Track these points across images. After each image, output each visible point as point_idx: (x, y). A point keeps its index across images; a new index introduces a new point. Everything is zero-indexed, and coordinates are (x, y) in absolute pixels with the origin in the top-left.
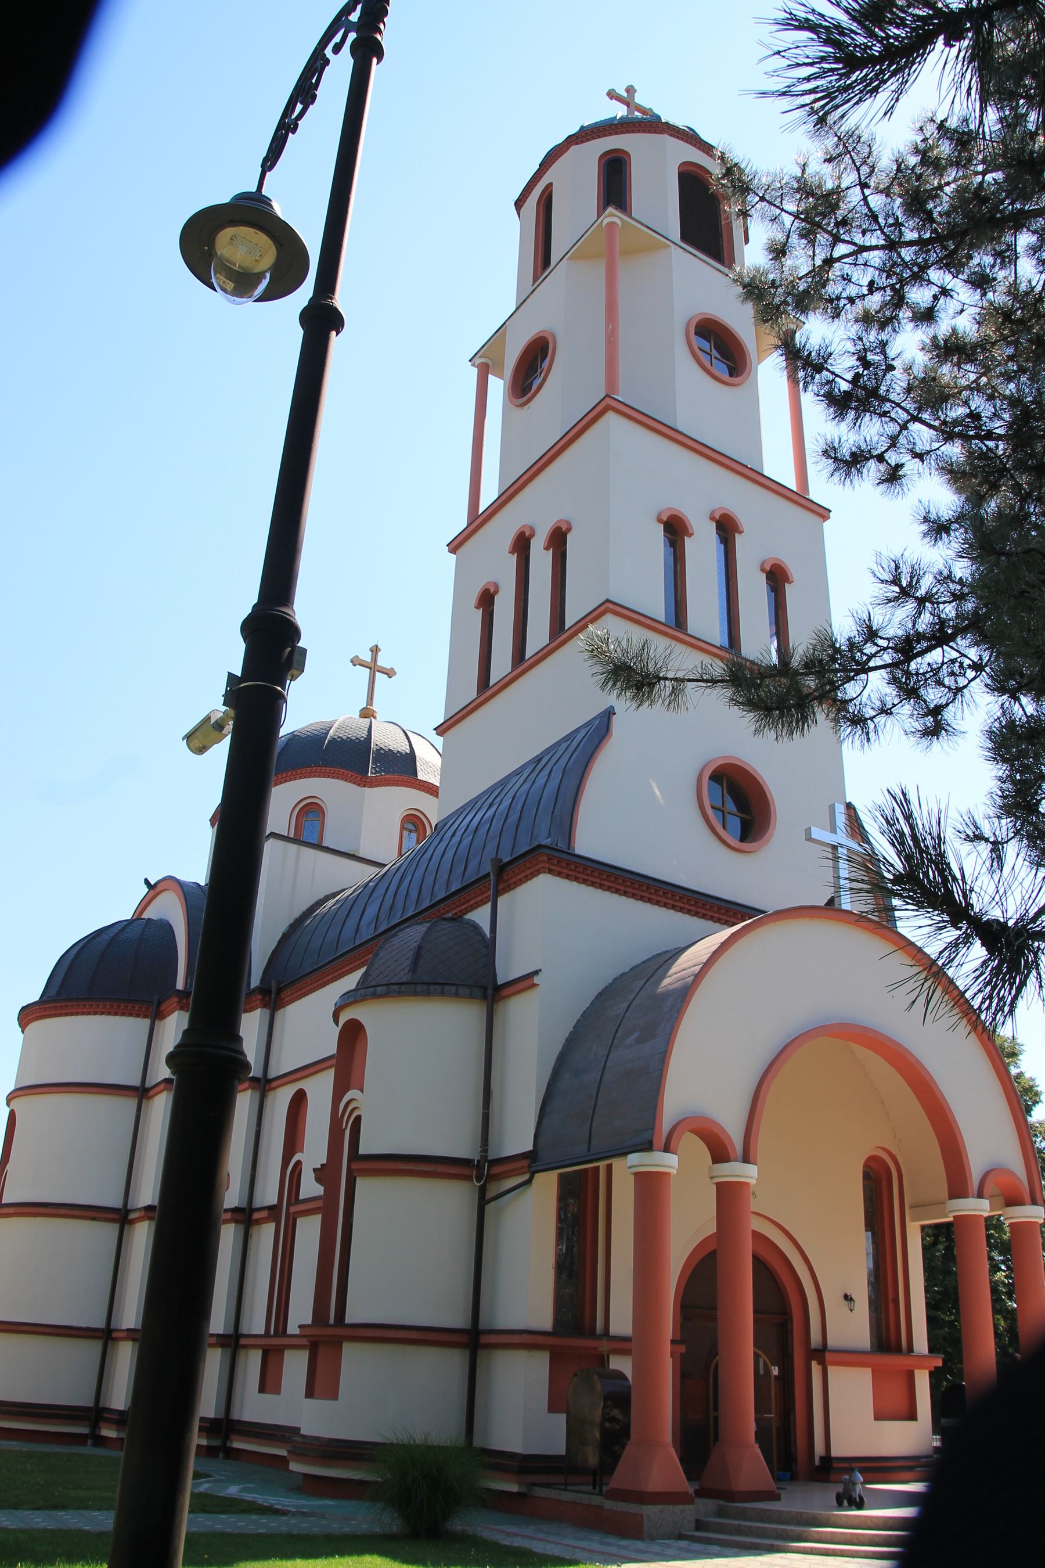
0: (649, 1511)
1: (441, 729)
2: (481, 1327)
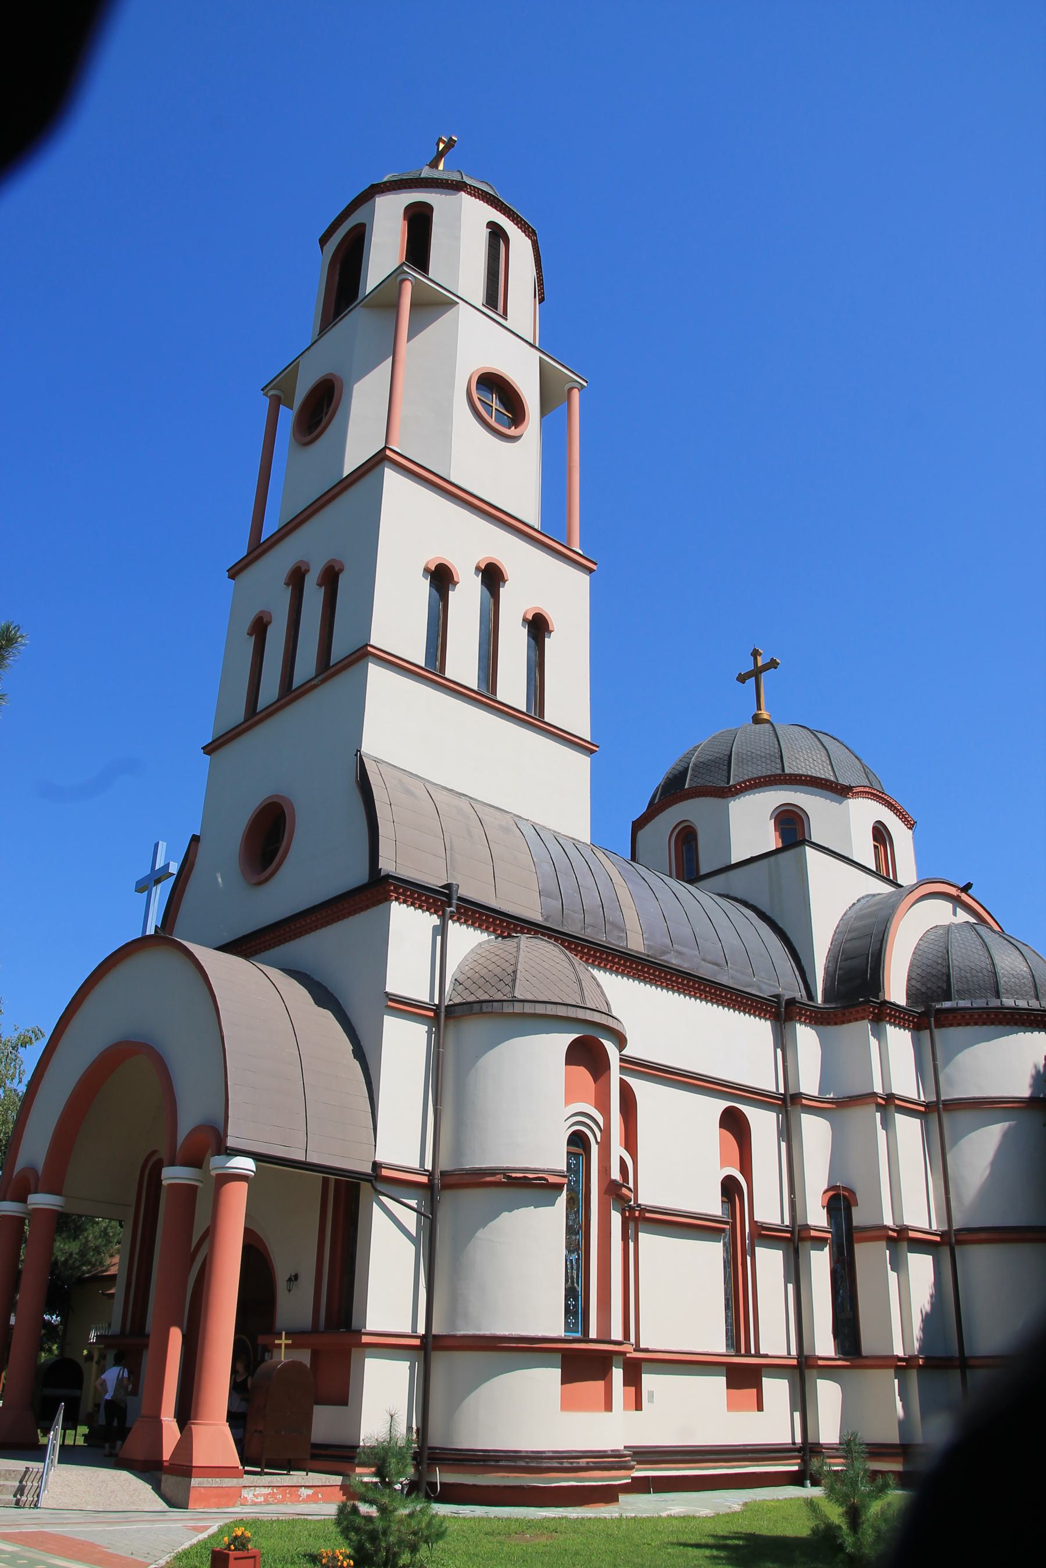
1: (210, 748)
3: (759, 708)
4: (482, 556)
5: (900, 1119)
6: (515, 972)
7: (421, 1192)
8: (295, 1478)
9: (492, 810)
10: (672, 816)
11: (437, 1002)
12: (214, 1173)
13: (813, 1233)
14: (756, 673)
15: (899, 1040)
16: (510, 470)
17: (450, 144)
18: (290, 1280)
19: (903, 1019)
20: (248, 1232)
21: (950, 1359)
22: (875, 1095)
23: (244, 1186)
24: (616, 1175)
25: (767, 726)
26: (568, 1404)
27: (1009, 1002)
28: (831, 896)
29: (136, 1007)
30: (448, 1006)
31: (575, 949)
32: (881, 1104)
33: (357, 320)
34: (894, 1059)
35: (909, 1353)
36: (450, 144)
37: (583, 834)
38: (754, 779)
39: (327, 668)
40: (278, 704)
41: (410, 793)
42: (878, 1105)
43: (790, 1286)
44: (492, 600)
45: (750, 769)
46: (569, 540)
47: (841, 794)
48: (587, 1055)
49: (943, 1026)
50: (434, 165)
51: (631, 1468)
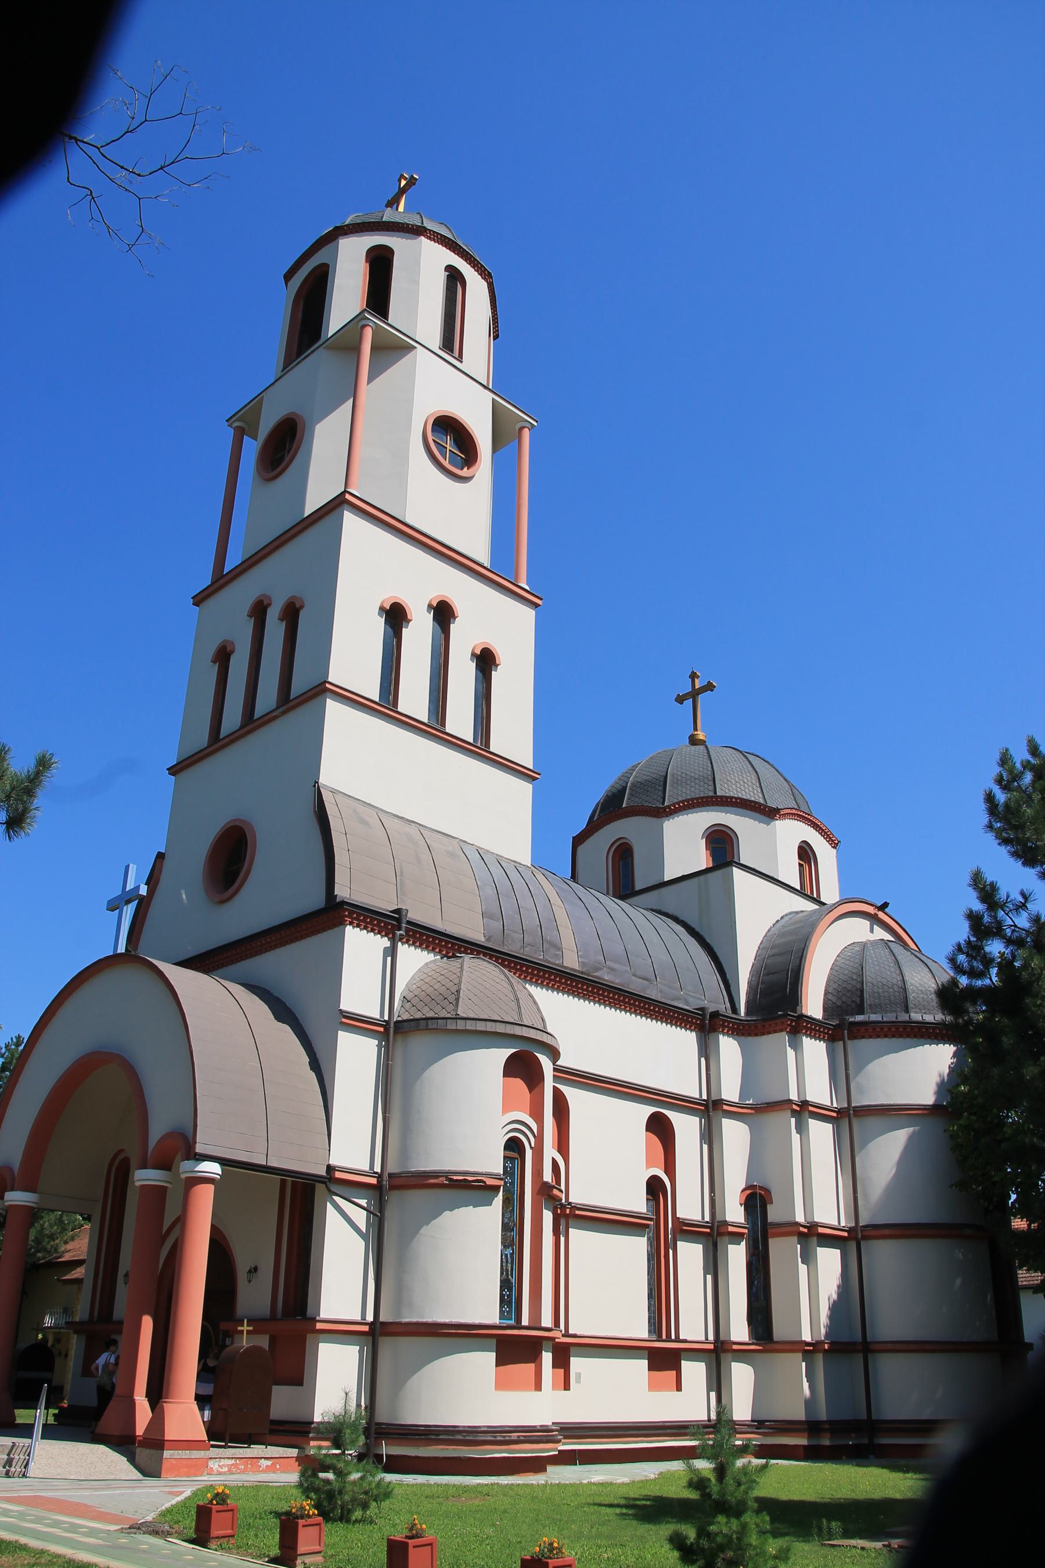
1: (174, 769)
3: (695, 729)
4: (434, 594)
5: (813, 1124)
6: (458, 991)
7: (370, 1192)
8: (256, 1451)
9: (439, 836)
10: (609, 834)
11: (386, 1018)
12: (183, 1176)
13: (730, 1229)
14: (694, 694)
15: (815, 1051)
16: (461, 510)
17: (412, 182)
18: (250, 1271)
19: (819, 1031)
20: (214, 1228)
21: (854, 1344)
22: (790, 1101)
23: (211, 1188)
24: (548, 1176)
25: (702, 747)
26: (501, 1384)
27: (916, 1016)
28: (757, 914)
29: (106, 1019)
30: (397, 1022)
31: (515, 968)
32: (796, 1111)
33: (318, 362)
34: (809, 1069)
35: (816, 1338)
36: (412, 182)
37: (525, 857)
38: (688, 800)
39: (288, 701)
40: (241, 732)
41: (363, 822)
42: (794, 1111)
43: (709, 1277)
44: (443, 636)
45: (684, 790)
46: (517, 577)
47: (769, 816)
48: (523, 1067)
49: (856, 1038)
50: (393, 203)
51: (559, 1441)
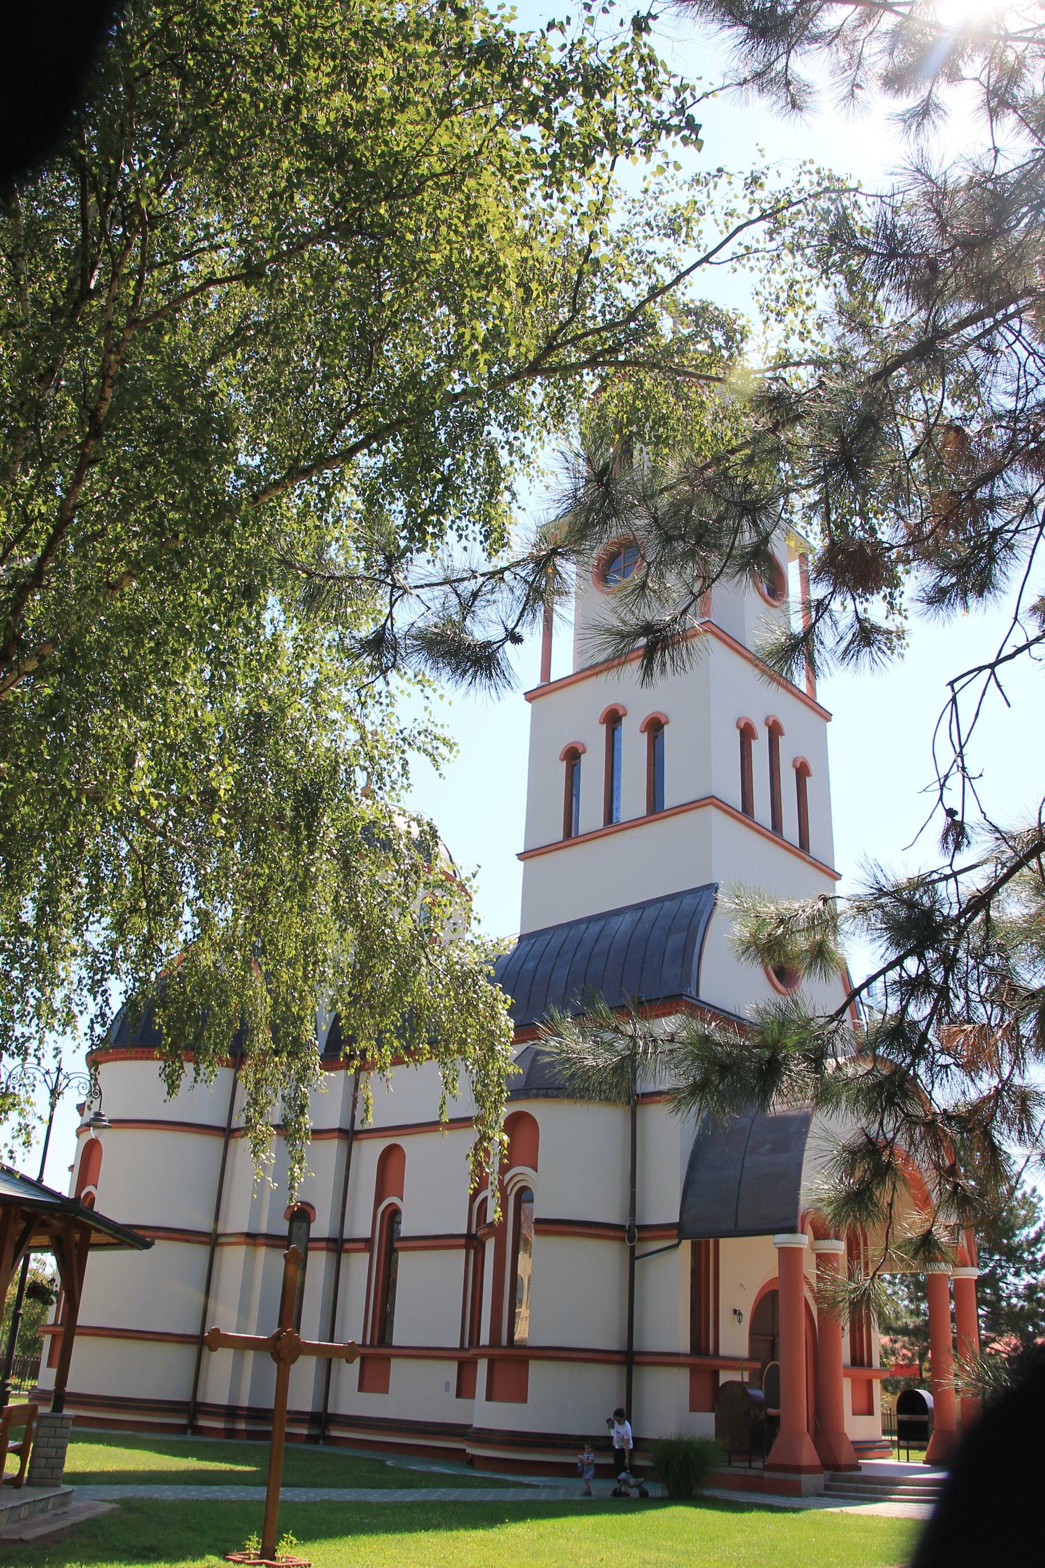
0: (804, 1478)
2: (635, 1348)
